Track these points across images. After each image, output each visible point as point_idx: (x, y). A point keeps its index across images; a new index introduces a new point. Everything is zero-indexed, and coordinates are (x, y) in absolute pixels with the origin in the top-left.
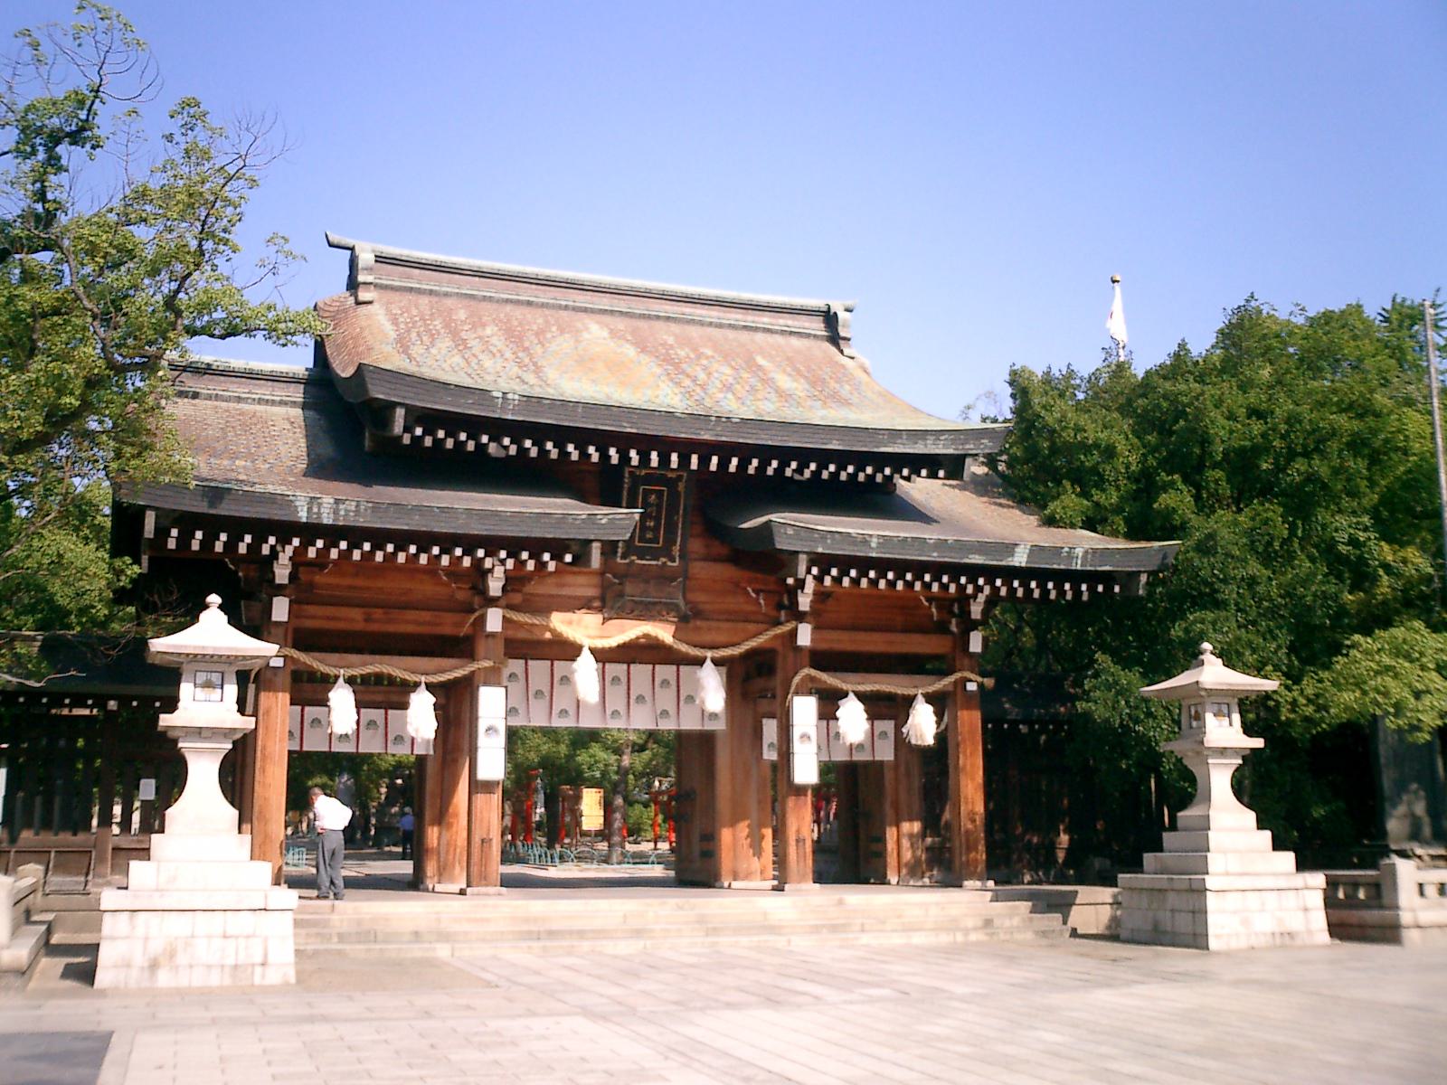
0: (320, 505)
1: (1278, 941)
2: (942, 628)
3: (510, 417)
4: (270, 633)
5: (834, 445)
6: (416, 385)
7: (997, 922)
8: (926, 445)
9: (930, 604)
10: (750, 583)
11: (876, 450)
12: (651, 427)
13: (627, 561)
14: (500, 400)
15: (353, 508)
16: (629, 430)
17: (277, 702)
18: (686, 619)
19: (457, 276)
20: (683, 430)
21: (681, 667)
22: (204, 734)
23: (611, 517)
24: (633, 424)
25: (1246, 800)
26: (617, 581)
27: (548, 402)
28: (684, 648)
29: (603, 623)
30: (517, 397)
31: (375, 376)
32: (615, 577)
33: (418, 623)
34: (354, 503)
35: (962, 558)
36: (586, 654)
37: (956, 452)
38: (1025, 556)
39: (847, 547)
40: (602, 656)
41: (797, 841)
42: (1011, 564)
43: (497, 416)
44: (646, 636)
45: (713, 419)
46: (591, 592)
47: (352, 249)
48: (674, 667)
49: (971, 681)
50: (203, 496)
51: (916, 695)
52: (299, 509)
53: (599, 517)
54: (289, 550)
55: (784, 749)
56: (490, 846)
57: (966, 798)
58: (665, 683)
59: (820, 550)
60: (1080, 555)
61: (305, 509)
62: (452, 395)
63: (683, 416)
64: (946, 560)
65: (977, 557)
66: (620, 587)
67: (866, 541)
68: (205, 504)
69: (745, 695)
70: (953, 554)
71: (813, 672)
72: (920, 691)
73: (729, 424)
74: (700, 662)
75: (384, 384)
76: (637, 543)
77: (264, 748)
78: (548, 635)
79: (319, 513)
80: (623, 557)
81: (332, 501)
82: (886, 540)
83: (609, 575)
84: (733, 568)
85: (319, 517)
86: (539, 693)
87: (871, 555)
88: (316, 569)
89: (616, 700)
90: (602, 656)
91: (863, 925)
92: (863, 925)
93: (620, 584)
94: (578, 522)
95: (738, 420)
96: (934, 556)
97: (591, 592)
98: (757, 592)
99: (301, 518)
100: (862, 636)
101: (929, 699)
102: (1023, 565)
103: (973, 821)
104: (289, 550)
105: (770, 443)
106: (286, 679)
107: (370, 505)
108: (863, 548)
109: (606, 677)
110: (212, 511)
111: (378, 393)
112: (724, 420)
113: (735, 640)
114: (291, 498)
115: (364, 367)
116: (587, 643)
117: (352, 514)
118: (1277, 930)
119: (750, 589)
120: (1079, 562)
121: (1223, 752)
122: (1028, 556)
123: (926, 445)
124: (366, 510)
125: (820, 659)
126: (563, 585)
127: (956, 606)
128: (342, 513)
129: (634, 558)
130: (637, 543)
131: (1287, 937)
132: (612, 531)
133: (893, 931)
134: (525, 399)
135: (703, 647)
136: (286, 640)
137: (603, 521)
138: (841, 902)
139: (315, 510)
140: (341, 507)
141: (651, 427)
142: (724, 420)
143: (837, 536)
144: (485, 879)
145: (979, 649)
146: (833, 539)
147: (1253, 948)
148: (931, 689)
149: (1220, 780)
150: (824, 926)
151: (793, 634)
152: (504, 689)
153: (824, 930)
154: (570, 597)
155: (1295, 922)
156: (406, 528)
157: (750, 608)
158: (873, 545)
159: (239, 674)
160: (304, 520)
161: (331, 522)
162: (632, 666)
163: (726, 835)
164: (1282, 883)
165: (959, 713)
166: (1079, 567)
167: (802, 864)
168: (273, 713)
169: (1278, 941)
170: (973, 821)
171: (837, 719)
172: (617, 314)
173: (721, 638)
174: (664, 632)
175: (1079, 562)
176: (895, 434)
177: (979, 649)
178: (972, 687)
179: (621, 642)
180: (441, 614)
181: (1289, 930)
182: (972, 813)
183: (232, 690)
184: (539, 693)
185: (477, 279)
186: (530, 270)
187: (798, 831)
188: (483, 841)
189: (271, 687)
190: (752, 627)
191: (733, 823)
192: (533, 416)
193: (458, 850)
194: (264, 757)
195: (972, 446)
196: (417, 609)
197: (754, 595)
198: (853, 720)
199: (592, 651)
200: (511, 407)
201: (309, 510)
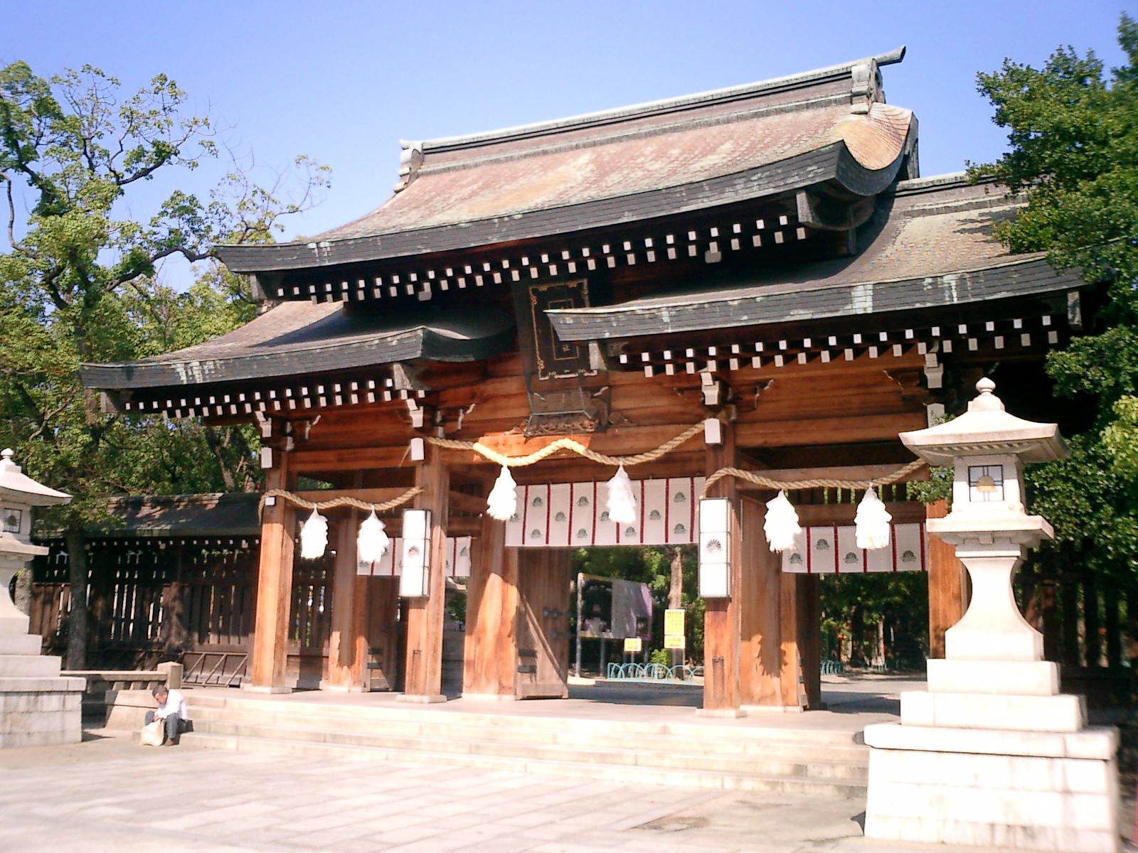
0: (191, 368)
1: (1000, 838)
3: (327, 264)
5: (627, 218)
7: (812, 770)
8: (736, 192)
11: (676, 211)
13: (547, 378)
14: (316, 251)
15: (212, 367)
16: (424, 251)
18: (603, 426)
21: (696, 479)
23: (399, 337)
24: (427, 245)
25: (1030, 613)
28: (598, 458)
30: (327, 244)
31: (226, 254)
33: (375, 458)
34: (212, 363)
35: (782, 316)
36: (505, 473)
37: (777, 191)
38: (870, 299)
40: (523, 476)
41: (715, 661)
42: (853, 312)
43: (317, 265)
45: (496, 221)
47: (122, 150)
48: (689, 480)
53: (389, 339)
54: (712, 366)
56: (420, 658)
57: (936, 612)
58: (680, 496)
59: (607, 335)
60: (953, 283)
62: (280, 256)
63: (469, 225)
64: (761, 322)
65: (801, 312)
67: (656, 317)
70: (772, 314)
71: (733, 471)
74: (606, 473)
75: (233, 258)
76: (555, 359)
77: (263, 571)
79: (193, 376)
80: (544, 374)
81: (198, 364)
82: (679, 312)
85: (194, 379)
86: (655, 514)
87: (666, 331)
89: (536, 520)
90: (523, 476)
91: (636, 757)
92: (636, 757)
94: (373, 348)
95: (520, 216)
96: (744, 320)
99: (182, 381)
102: (870, 311)
104: (712, 366)
105: (558, 232)
106: (278, 513)
107: (222, 362)
108: (654, 326)
112: (506, 219)
114: (173, 366)
117: (213, 372)
118: (1001, 819)
120: (955, 294)
121: (995, 538)
122: (874, 300)
123: (736, 192)
124: (221, 366)
126: (496, 409)
128: (207, 372)
129: (554, 373)
130: (555, 359)
131: (1020, 835)
132: (402, 352)
133: (673, 768)
134: (333, 245)
135: (617, 456)
136: (280, 483)
137: (394, 343)
138: (665, 731)
139: (190, 373)
140: (205, 367)
142: (506, 219)
143: (621, 316)
144: (415, 687)
146: (618, 321)
147: (943, 843)
148: (794, 486)
149: (993, 580)
150: (591, 755)
153: (592, 760)
155: (1044, 812)
156: (250, 377)
158: (666, 319)
160: (185, 383)
161: (202, 381)
164: (1053, 747)
166: (956, 301)
167: (719, 688)
169: (1000, 838)
171: (855, 525)
172: (624, 139)
173: (642, 444)
174: (578, 447)
175: (955, 294)
176: (693, 188)
179: (539, 458)
180: (356, 450)
181: (1026, 822)
184: (655, 514)
186: (561, 121)
187: (715, 652)
189: (270, 521)
190: (672, 428)
192: (344, 259)
193: (485, 663)
195: (797, 178)
196: (318, 450)
198: (782, 523)
199: (509, 468)
200: (326, 255)
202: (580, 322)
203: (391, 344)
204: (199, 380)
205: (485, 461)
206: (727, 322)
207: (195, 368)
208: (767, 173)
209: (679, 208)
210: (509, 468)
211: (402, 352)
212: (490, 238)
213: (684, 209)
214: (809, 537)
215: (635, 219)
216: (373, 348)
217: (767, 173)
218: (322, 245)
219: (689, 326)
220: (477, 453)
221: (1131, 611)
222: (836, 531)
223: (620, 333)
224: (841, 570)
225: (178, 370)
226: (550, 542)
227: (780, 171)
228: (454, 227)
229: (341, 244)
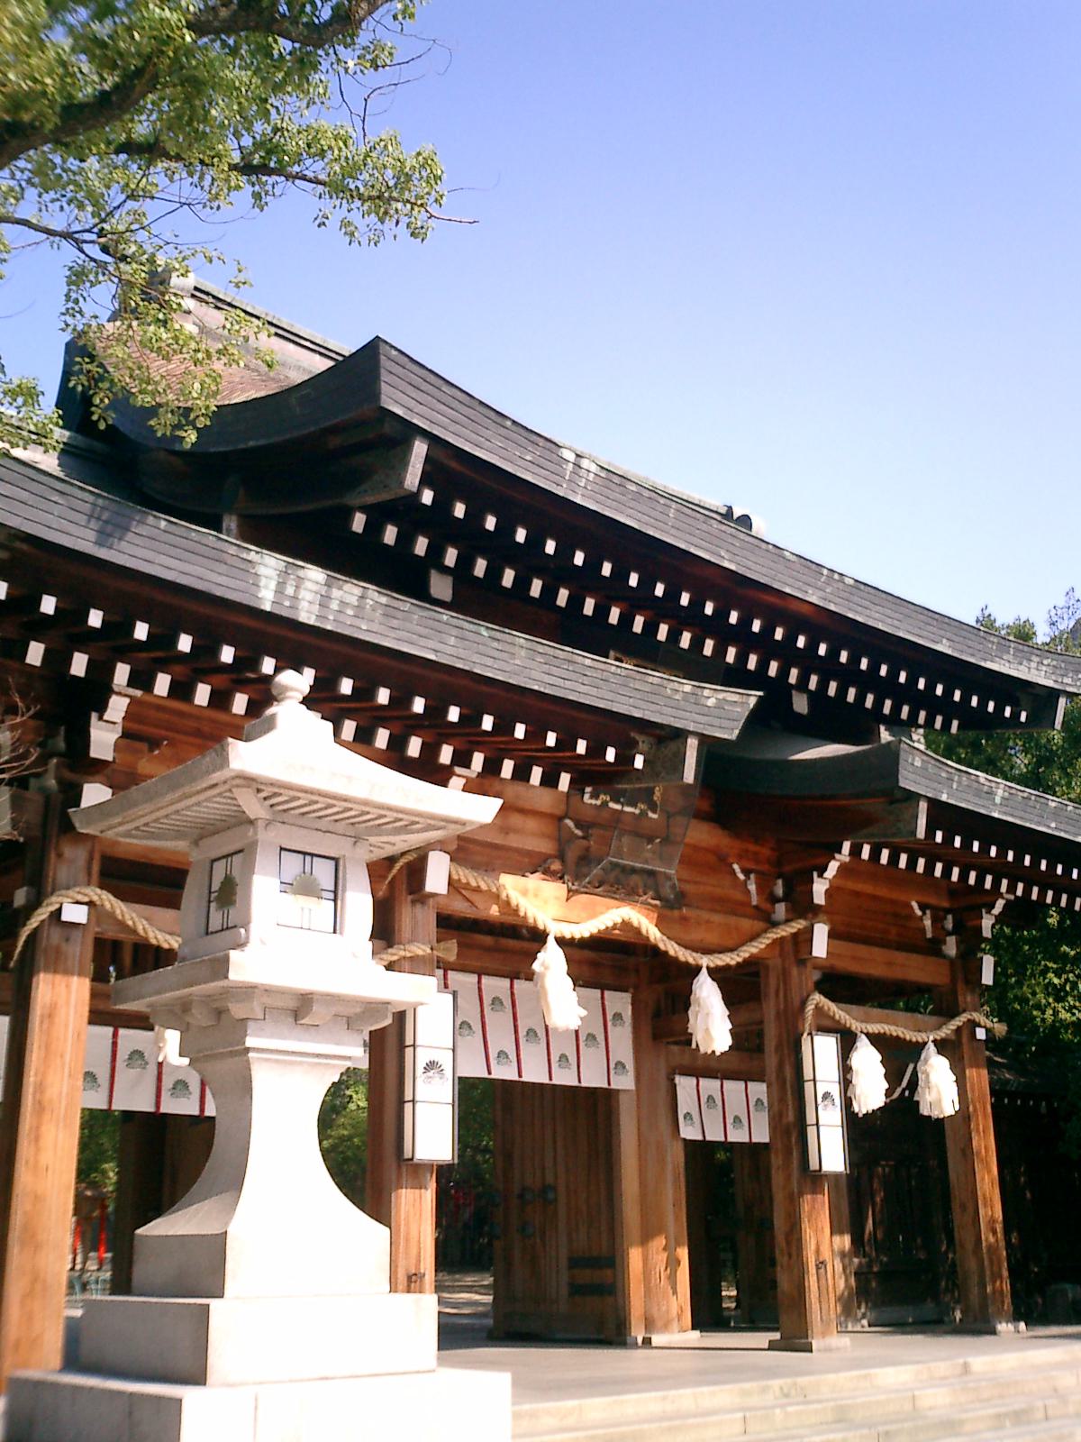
2: (933, 948)
4: (60, 855)
6: (455, 404)
9: (924, 913)
10: (739, 859)
12: (758, 568)
15: (354, 600)
17: (69, 993)
19: (291, 346)
20: (790, 581)
22: (318, 1013)
23: (721, 696)
26: (579, 832)
27: (633, 488)
29: (567, 899)
32: (577, 826)
39: (970, 797)
44: (626, 925)
45: (825, 572)
46: (544, 846)
49: (980, 1026)
50: (91, 516)
51: (925, 1043)
52: (263, 582)
53: (706, 693)
55: (791, 1116)
57: (984, 1196)
59: (944, 798)
61: (273, 585)
63: (793, 558)
66: (584, 842)
68: (92, 535)
69: (657, 1037)
72: (931, 1038)
73: (841, 586)
77: (40, 1087)
78: (494, 911)
83: (569, 822)
84: (719, 832)
88: (144, 746)
93: (583, 838)
95: (852, 582)
97: (544, 846)
98: (746, 872)
100: (862, 950)
101: (942, 1047)
103: (994, 1232)
106: (81, 950)
108: (986, 803)
109: (484, 997)
110: (103, 553)
111: (395, 400)
113: (730, 943)
115: (383, 348)
116: (555, 929)
117: (350, 612)
119: (736, 867)
125: (839, 985)
127: (950, 917)
128: (334, 605)
132: (717, 722)
134: (603, 474)
136: (89, 874)
138: (966, 1369)
139: (290, 591)
141: (753, 566)
142: (836, 576)
145: (990, 983)
151: (805, 938)
152: (451, 997)
154: (517, 850)
157: (738, 896)
159: (378, 870)
161: (312, 621)
162: (516, 981)
163: (635, 1256)
165: (967, 1072)
168: (61, 1014)
170: (994, 1232)
177: (990, 983)
178: (981, 1034)
182: (992, 1221)
183: (359, 905)
185: (318, 357)
187: (818, 1251)
188: (409, 1278)
191: (645, 1239)
194: (40, 1108)
197: (741, 877)
201: (280, 591)
202: (927, 769)
203: (703, 701)
204: (307, 616)
205: (510, 919)
206: (1039, 823)
207: (308, 585)
208: (1055, 663)
209: (985, 660)
210: (561, 942)
211: (717, 722)
212: (810, 592)
213: (989, 665)
214: (115, 1044)
215: (949, 652)
216: (677, 697)
217: (1055, 663)
218: (585, 463)
219: (1012, 815)
220: (496, 897)
221: (1079, 1175)
222: (115, 1035)
223: (957, 799)
224: (114, 1107)
225: (262, 570)
226: (523, 1074)
227: (1063, 665)
228: (777, 551)
229: (617, 479)
